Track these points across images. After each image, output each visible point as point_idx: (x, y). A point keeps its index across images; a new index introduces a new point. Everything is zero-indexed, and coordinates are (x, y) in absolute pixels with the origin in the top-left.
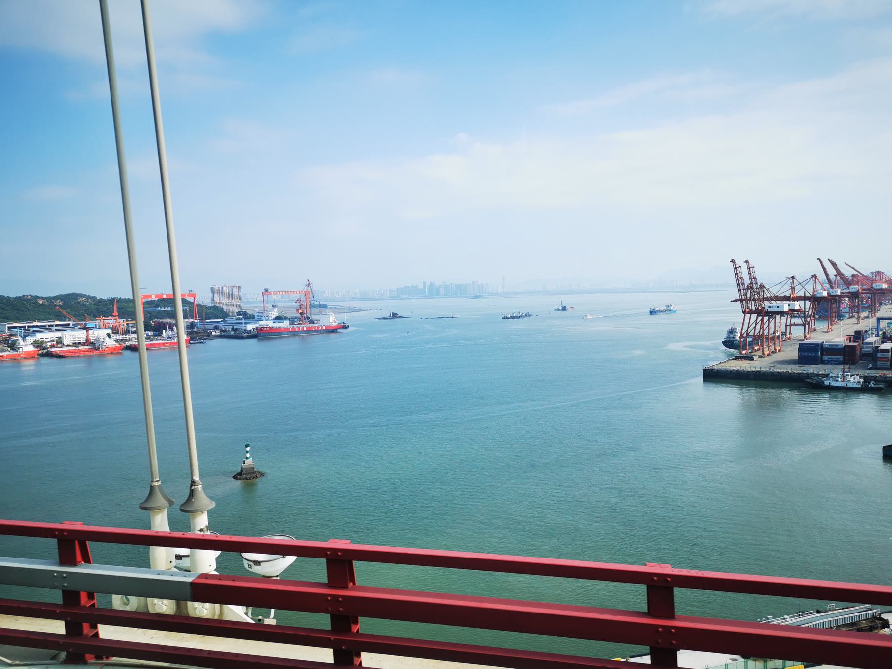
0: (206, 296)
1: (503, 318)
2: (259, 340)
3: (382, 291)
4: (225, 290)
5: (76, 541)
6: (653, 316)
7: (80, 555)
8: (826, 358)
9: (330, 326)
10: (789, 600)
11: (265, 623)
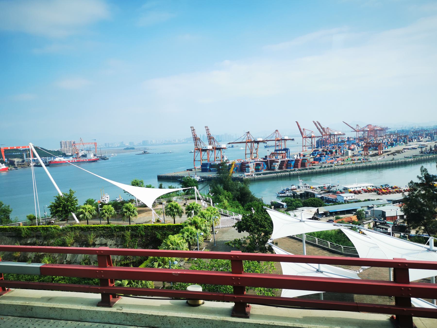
2: (50, 167)
4: (67, 143)
9: (91, 159)
10: (377, 271)
11: (281, 296)
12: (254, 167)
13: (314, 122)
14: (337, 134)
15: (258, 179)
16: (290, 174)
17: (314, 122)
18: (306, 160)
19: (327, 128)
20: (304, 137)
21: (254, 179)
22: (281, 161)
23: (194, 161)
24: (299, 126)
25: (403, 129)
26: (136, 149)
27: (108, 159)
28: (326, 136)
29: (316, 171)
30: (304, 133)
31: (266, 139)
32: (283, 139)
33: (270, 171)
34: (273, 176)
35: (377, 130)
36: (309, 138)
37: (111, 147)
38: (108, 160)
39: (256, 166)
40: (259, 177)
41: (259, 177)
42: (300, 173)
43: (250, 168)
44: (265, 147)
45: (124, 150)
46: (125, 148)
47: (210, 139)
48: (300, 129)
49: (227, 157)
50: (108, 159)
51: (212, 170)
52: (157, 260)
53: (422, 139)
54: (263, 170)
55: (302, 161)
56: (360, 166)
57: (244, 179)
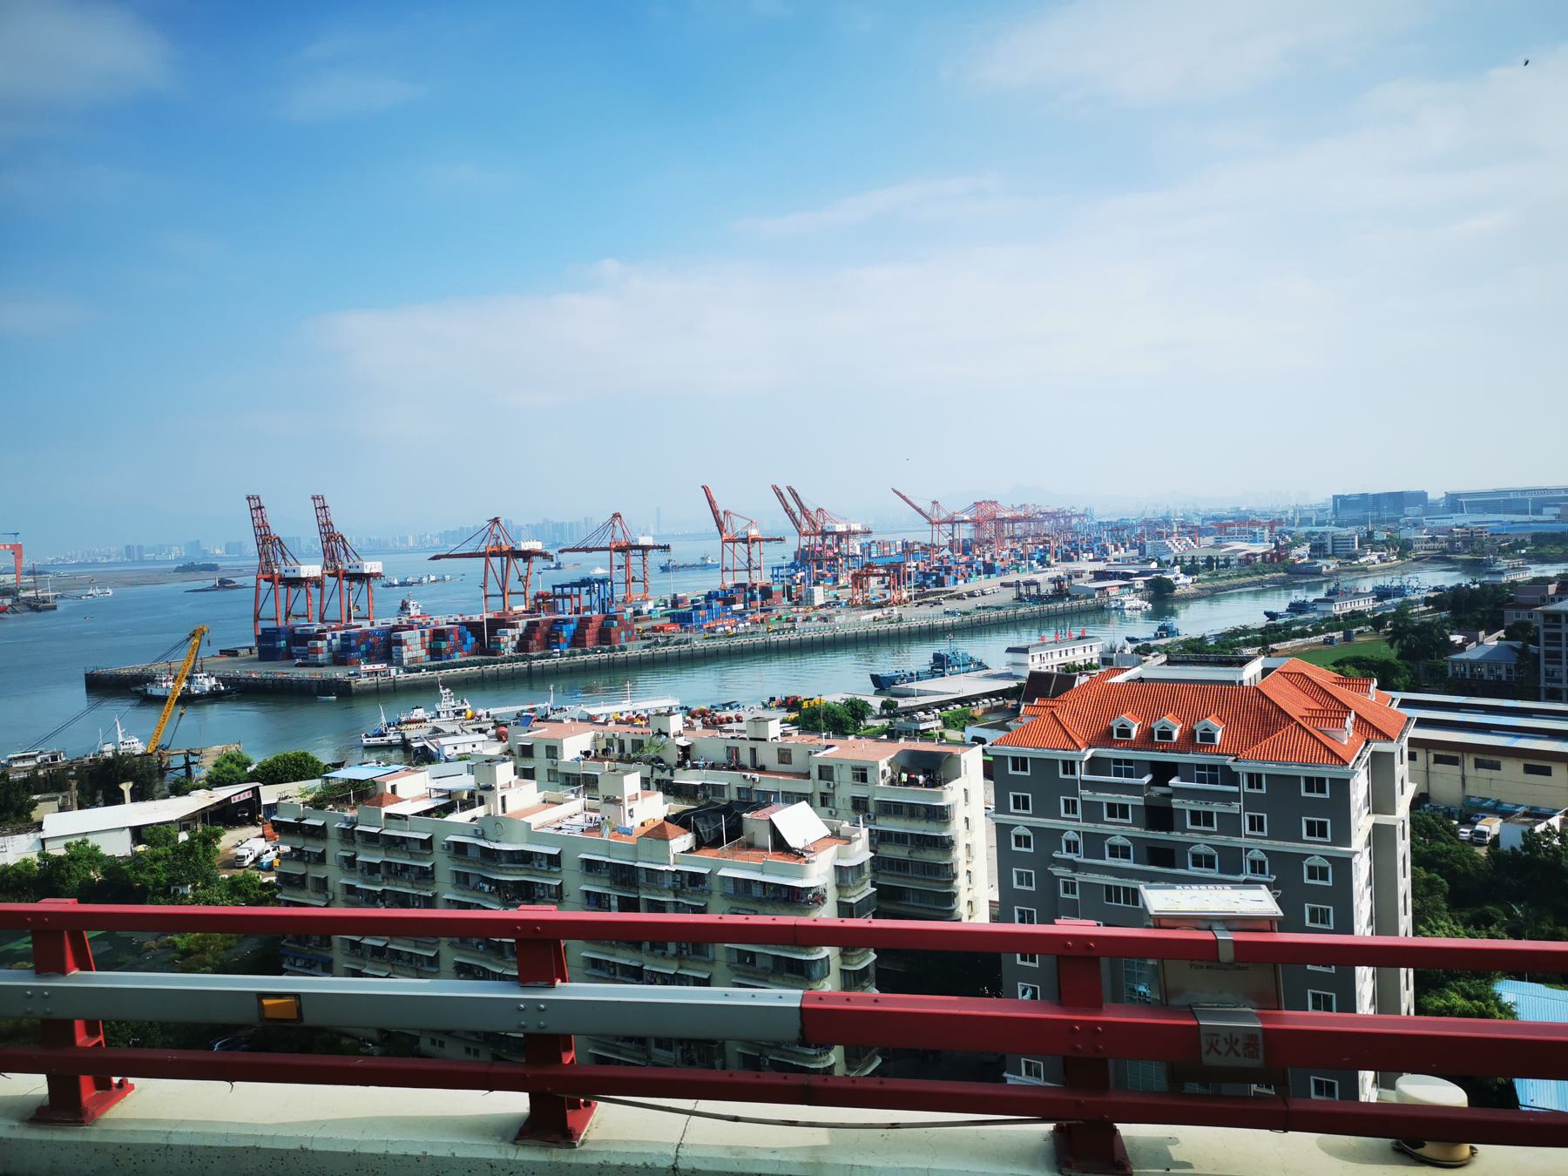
0: (97, 550)
1: (383, 586)
3: (428, 537)
5: (66, 932)
6: (666, 574)
7: (72, 958)
8: (295, 651)
12: (423, 643)
13: (775, 488)
14: (845, 530)
15: (408, 685)
16: (530, 668)
17: (775, 488)
18: (616, 620)
19: (820, 510)
20: (727, 541)
21: (394, 686)
22: (529, 624)
23: (256, 621)
24: (711, 502)
25: (1146, 516)
26: (224, 571)
27: (54, 608)
28: (812, 537)
29: (624, 656)
30: (727, 526)
31: (585, 545)
32: (635, 544)
33: (484, 658)
34: (467, 674)
35: (1003, 520)
36: (741, 544)
37: (154, 561)
38: (52, 612)
39: (434, 640)
40: (411, 680)
41: (414, 679)
42: (567, 666)
43: (404, 648)
44: (661, 568)
45: (175, 571)
46: (181, 565)
47: (332, 541)
48: (715, 513)
49: (418, 608)
50: (54, 608)
51: (296, 654)
52: (694, 885)
53: (1117, 553)
54: (457, 654)
55: (603, 624)
56: (780, 639)
57: (353, 685)
